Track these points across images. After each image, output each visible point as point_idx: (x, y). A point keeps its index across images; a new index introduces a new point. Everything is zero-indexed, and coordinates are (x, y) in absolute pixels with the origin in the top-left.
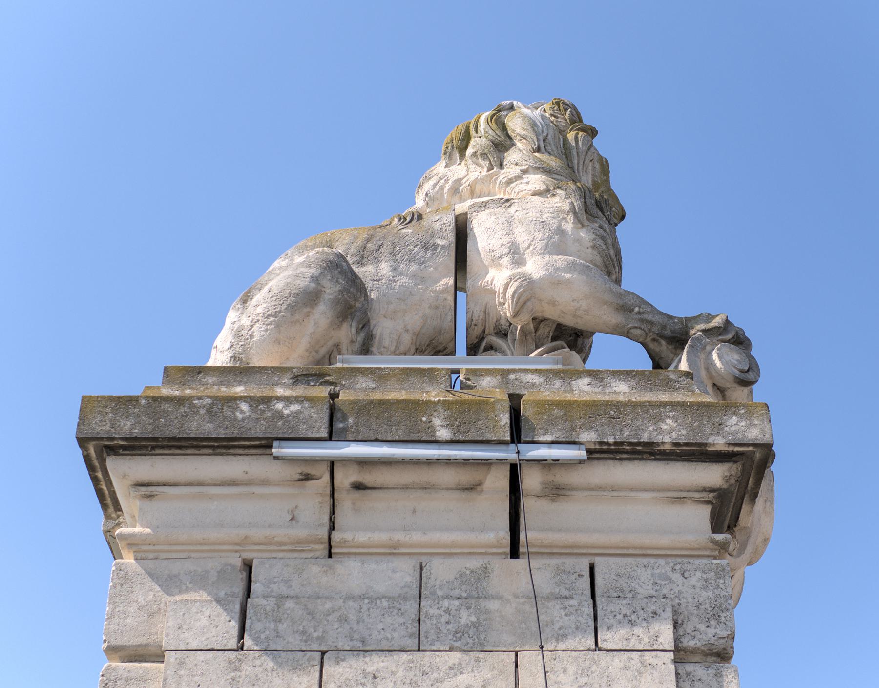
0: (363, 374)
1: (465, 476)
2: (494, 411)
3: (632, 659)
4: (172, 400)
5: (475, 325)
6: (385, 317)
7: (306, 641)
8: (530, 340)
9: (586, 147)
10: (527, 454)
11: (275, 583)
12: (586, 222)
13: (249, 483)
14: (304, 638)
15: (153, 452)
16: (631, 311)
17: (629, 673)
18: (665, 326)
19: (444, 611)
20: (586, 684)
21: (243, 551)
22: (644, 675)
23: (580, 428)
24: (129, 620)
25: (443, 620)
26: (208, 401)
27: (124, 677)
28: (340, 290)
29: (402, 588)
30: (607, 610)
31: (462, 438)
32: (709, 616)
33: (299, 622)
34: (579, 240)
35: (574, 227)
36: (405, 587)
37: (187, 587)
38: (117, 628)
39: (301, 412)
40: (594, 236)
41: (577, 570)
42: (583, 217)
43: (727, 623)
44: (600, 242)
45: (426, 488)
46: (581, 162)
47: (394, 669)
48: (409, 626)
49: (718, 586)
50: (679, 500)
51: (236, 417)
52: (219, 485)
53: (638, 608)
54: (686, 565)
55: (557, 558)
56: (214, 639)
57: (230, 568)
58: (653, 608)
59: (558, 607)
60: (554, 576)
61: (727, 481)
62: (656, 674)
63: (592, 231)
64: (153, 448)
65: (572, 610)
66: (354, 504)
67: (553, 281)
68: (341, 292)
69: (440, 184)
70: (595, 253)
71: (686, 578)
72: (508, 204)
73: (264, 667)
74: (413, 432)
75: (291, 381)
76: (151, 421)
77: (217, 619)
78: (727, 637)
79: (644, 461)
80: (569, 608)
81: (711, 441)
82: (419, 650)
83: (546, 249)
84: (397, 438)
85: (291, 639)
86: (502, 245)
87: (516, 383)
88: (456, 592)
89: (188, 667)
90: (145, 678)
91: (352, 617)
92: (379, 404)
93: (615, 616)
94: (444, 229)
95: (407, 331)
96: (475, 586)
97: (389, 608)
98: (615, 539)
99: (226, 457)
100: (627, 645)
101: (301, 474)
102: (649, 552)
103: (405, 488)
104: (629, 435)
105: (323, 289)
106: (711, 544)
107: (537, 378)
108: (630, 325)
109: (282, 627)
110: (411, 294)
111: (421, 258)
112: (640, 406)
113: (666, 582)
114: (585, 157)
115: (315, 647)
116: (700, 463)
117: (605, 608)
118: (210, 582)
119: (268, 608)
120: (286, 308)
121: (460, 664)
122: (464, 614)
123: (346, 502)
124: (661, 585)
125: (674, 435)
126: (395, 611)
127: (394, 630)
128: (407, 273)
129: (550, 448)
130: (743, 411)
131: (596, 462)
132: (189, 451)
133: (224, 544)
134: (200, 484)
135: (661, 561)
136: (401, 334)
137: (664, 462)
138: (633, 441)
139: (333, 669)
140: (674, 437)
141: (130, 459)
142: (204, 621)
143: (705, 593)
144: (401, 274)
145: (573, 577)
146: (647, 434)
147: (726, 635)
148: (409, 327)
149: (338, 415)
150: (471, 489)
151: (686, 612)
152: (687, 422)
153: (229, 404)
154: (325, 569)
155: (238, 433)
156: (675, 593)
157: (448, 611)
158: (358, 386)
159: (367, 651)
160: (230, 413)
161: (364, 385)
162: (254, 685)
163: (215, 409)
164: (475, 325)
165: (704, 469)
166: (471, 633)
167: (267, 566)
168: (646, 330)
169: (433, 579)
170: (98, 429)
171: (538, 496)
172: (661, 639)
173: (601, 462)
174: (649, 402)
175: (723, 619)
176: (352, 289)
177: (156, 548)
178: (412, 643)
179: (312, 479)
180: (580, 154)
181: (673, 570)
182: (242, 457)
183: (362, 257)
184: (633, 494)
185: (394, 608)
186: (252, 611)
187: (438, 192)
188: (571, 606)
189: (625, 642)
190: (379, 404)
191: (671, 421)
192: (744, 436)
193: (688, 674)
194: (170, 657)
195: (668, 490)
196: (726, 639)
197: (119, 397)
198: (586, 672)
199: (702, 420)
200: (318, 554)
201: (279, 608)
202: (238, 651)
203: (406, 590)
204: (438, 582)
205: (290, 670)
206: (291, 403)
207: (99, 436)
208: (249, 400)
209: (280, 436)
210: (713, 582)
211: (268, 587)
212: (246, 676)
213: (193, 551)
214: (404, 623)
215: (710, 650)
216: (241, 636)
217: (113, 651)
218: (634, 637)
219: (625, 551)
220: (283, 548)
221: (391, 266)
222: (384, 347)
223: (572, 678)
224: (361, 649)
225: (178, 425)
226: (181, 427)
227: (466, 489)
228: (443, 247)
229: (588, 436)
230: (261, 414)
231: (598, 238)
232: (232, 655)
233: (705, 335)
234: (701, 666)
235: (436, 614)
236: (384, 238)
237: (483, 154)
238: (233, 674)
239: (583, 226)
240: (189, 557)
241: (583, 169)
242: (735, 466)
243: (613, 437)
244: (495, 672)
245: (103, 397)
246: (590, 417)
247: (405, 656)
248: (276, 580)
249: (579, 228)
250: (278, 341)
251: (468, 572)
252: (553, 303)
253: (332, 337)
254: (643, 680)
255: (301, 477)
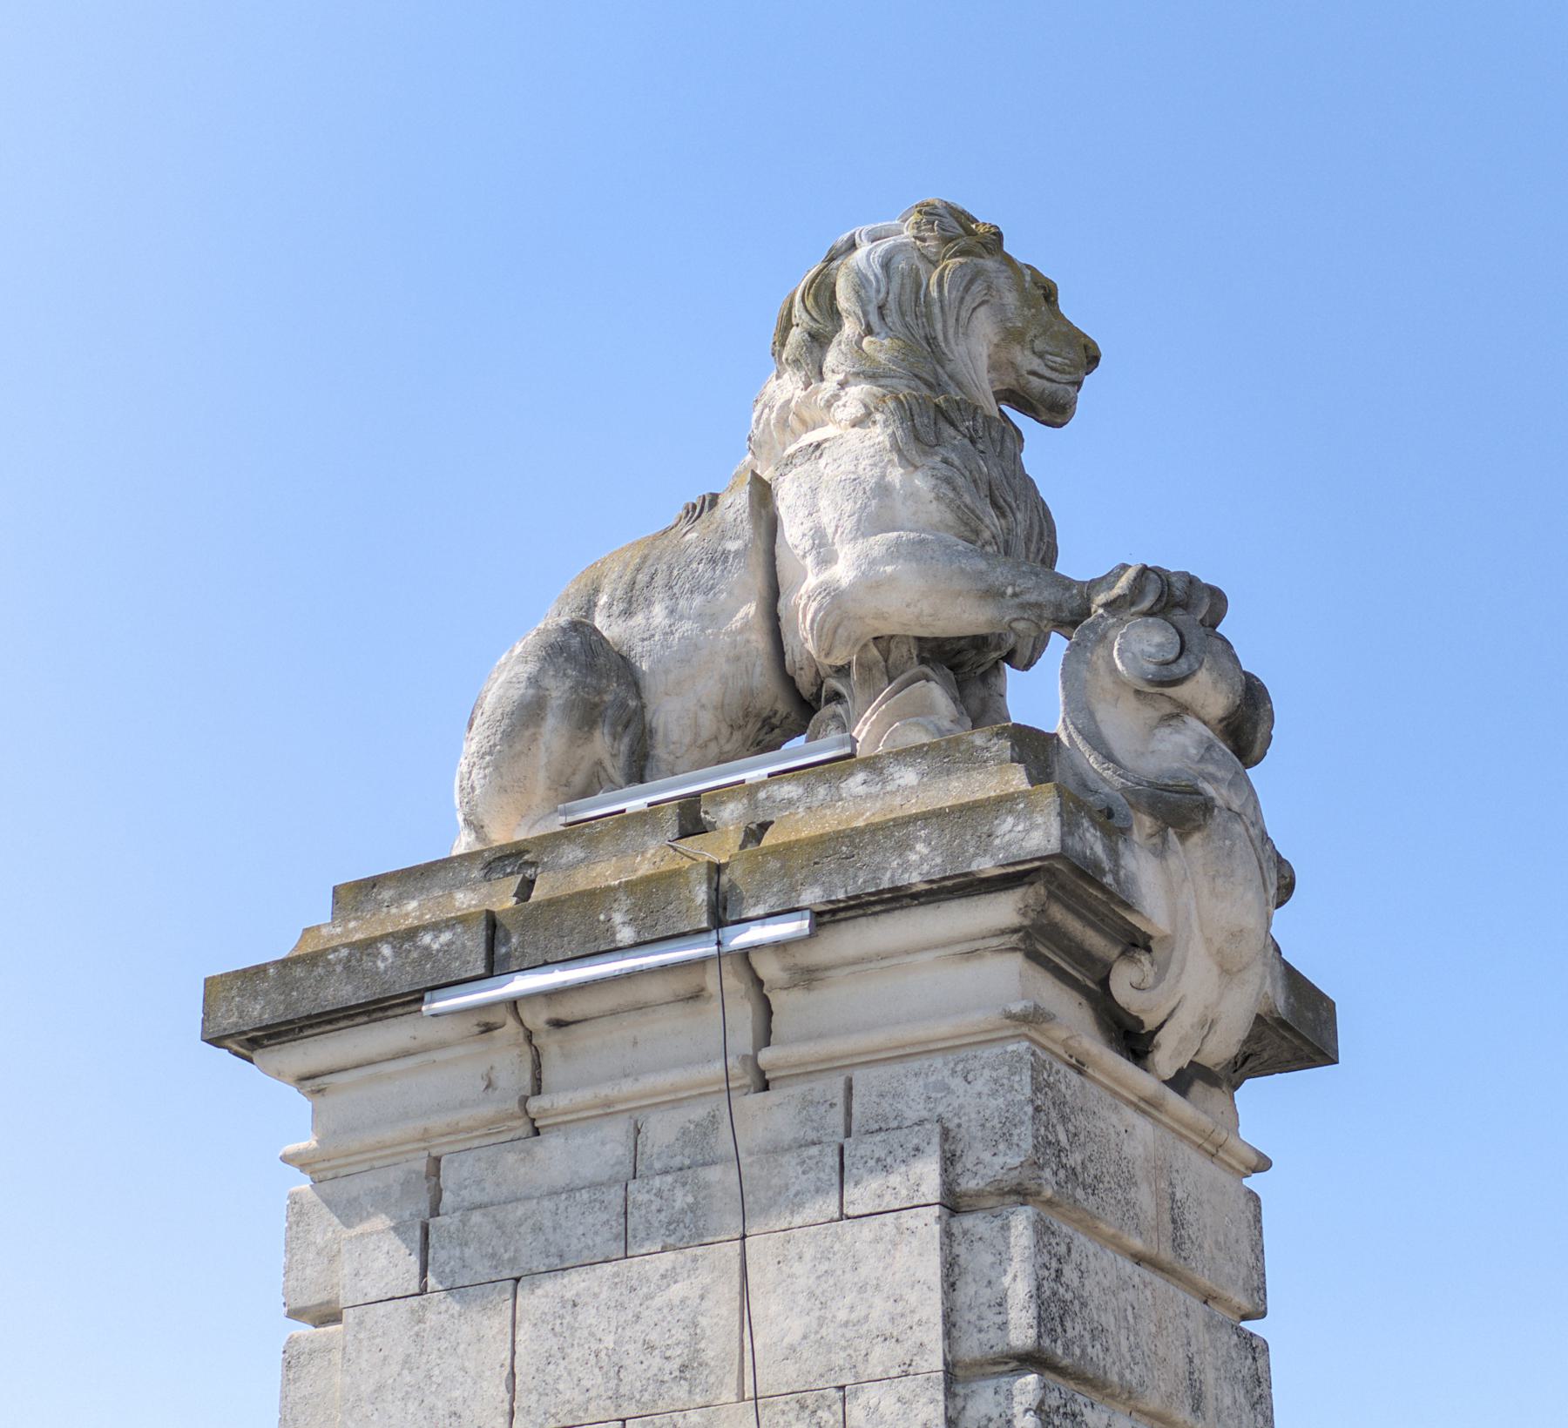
0: (569, 841)
1: (680, 984)
2: (687, 884)
3: (885, 1225)
4: (304, 961)
5: (801, 669)
6: (667, 694)
7: (496, 1268)
8: (878, 675)
9: (958, 290)
10: (731, 944)
11: (466, 1188)
12: (917, 461)
13: (425, 1049)
14: (494, 1263)
15: (301, 1034)
16: (1003, 595)
17: (881, 1247)
18: (1060, 605)
19: (655, 1194)
20: (826, 1272)
21: (432, 1146)
22: (899, 1247)
23: (802, 884)
24: (308, 1271)
25: (654, 1208)
26: (344, 952)
27: (307, 1350)
28: (571, 688)
29: (613, 1166)
30: (855, 1156)
31: (648, 937)
32: (996, 1137)
33: (488, 1242)
34: (913, 495)
35: (905, 474)
36: (616, 1164)
37: (368, 1212)
38: (295, 1284)
39: (453, 943)
40: (934, 482)
41: (829, 1097)
42: (913, 454)
43: (1021, 1143)
44: (945, 489)
45: (640, 1007)
46: (951, 322)
47: (596, 1290)
48: (613, 1223)
49: (1012, 1087)
50: (971, 954)
51: (377, 968)
52: (393, 1059)
53: (895, 1146)
54: (971, 1062)
55: (789, 1086)
56: (394, 1283)
57: (414, 1176)
58: (916, 1141)
59: (794, 1163)
60: (799, 1113)
61: (1024, 915)
62: (915, 1243)
63: (929, 473)
64: (301, 1029)
65: (811, 1163)
66: (561, 1047)
67: (871, 583)
68: (573, 689)
69: (765, 416)
70: (943, 508)
71: (969, 1083)
72: (818, 453)
73: (451, 1312)
74: (589, 942)
75: (482, 873)
76: (283, 997)
77: (396, 1254)
78: (1021, 1166)
79: (907, 910)
80: (808, 1161)
81: (974, 867)
82: (626, 1257)
83: (858, 529)
84: (570, 955)
85: (479, 1268)
86: (804, 535)
87: (768, 804)
88: (677, 1162)
89: (368, 1327)
90: (329, 1347)
91: (548, 1223)
92: (548, 906)
93: (866, 1162)
94: (739, 519)
95: (703, 706)
96: (700, 1146)
97: (590, 1202)
98: (878, 1039)
99: (385, 1022)
100: (880, 1205)
101: (478, 1025)
102: (932, 1047)
103: (614, 1013)
104: (865, 882)
105: (547, 693)
106: (1008, 1021)
107: (794, 788)
108: (1007, 618)
109: (468, 1252)
110: (696, 647)
111: (708, 581)
112: (882, 829)
113: (943, 1094)
114: (960, 308)
115: (506, 1274)
116: (983, 896)
117: (853, 1153)
118: (393, 1200)
119: (452, 1228)
120: (501, 739)
121: (674, 1268)
122: (679, 1193)
123: (551, 1044)
124: (936, 1100)
125: (925, 868)
126: (598, 1205)
127: (596, 1233)
128: (689, 614)
129: (763, 925)
130: (1022, 806)
131: (843, 925)
132: (342, 1024)
133: (408, 1143)
134: (371, 1063)
135: (938, 1062)
136: (696, 714)
137: (932, 905)
138: (870, 890)
139: (526, 1301)
140: (924, 872)
141: (279, 1050)
142: (382, 1261)
143: (994, 1102)
144: (681, 618)
145: (822, 1109)
146: (888, 874)
147: (1018, 1164)
148: (704, 701)
149: (500, 934)
150: (697, 996)
151: (967, 1136)
152: (945, 841)
153: (370, 951)
154: (522, 1155)
155: (380, 994)
156: (954, 1108)
157: (659, 1194)
158: (563, 861)
159: (567, 1269)
160: (370, 964)
161: (571, 856)
162: (440, 1339)
163: (354, 963)
164: (801, 669)
165: (977, 906)
166: (687, 1221)
167: (456, 1165)
168: (1034, 619)
169: (649, 1146)
170: (225, 1023)
171: (786, 989)
172: (923, 1189)
173: (851, 924)
174: (894, 820)
175: (1015, 1138)
176: (588, 680)
177: (333, 1163)
178: (616, 1249)
179: (496, 1028)
180: (947, 308)
181: (954, 1072)
182: (403, 1018)
183: (630, 603)
184: (908, 959)
185: (595, 1200)
186: (434, 1236)
187: (763, 430)
188: (810, 1158)
189: (877, 1201)
190: (548, 906)
191: (922, 845)
192: (1021, 847)
193: (965, 1233)
194: (348, 1316)
195: (944, 945)
196: (1019, 1169)
197: (245, 971)
198: (825, 1255)
199: (965, 835)
200: (519, 1133)
201: (464, 1225)
202: (421, 1294)
203: (617, 1168)
204: (656, 1149)
205: (479, 1312)
206: (441, 932)
207: (226, 1033)
208: (391, 939)
209: (429, 985)
210: (1005, 1081)
211: (459, 1195)
212: (431, 1328)
213: (374, 1159)
214: (608, 1221)
215: (999, 1189)
216: (424, 1274)
217: (295, 1314)
218: (890, 1191)
219: (901, 1052)
220: (475, 1134)
221: (667, 608)
222: (674, 743)
223: (810, 1265)
224: (559, 1267)
225: (313, 997)
226: (316, 999)
227: (691, 998)
228: (737, 553)
229: (812, 896)
230: (406, 957)
231: (939, 482)
232: (414, 1301)
233: (1109, 612)
234: (984, 1218)
235: (645, 1200)
236: (659, 559)
237: (794, 361)
238: (416, 1328)
239: (916, 468)
240: (372, 1168)
241: (956, 333)
242: (1031, 890)
243: (843, 890)
244: (716, 1274)
245: (227, 975)
246: (816, 863)
247: (609, 1268)
248: (467, 1183)
249: (913, 472)
250: (503, 790)
251: (692, 1127)
252: (880, 616)
253: (582, 757)
254: (898, 1255)
255: (482, 1029)
